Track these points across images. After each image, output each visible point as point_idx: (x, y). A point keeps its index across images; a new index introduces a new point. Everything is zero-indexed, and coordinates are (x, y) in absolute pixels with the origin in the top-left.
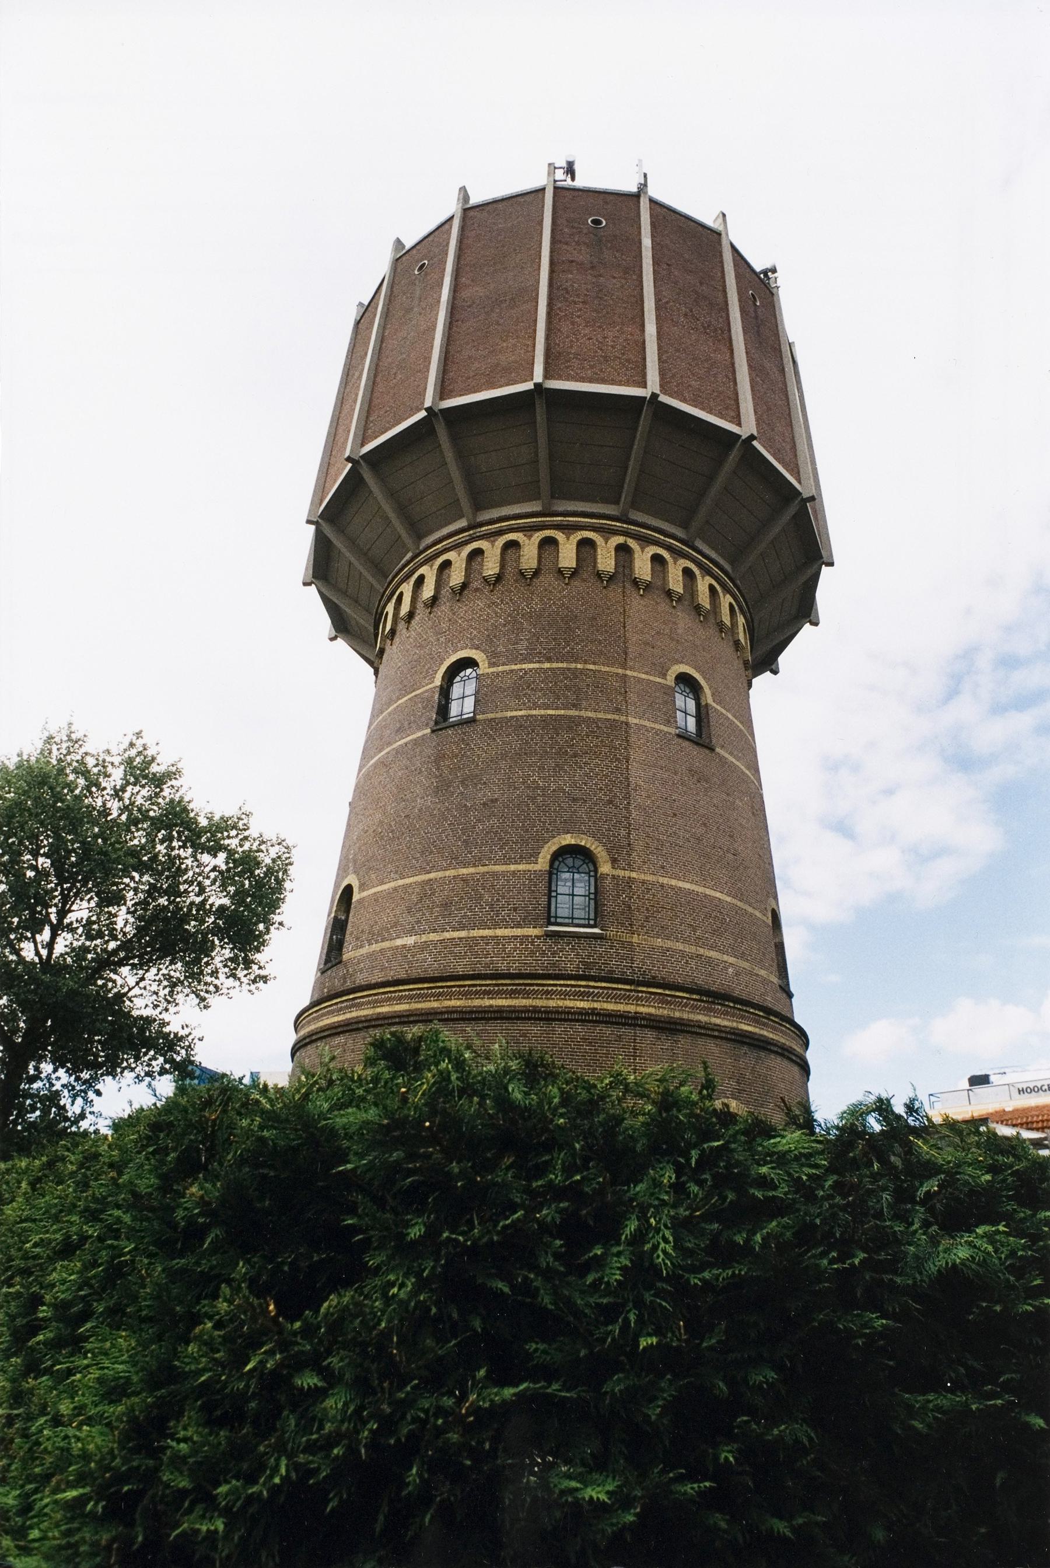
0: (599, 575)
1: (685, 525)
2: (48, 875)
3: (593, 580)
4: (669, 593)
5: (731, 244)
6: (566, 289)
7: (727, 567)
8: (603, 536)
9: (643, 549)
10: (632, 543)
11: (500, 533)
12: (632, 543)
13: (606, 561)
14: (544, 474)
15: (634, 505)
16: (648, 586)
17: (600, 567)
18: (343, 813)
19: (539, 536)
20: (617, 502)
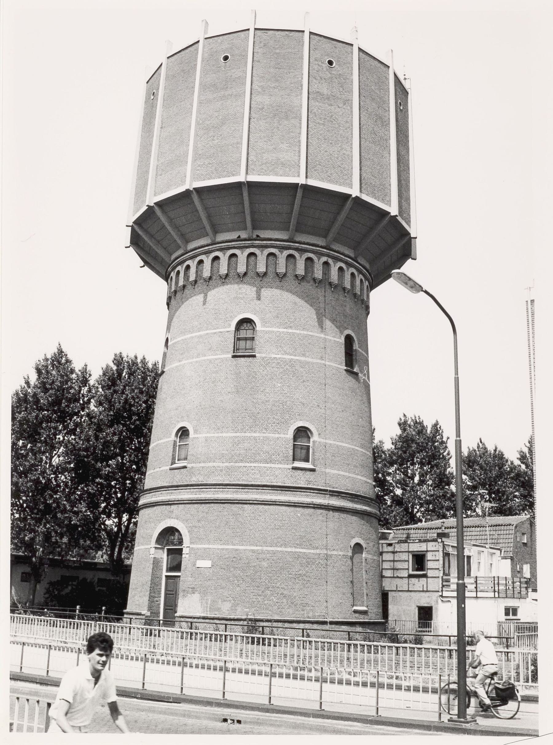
0: (314, 280)
1: (355, 248)
2: (141, 477)
3: (312, 282)
4: (344, 289)
5: (395, 75)
6: (315, 113)
7: (368, 266)
8: (317, 257)
9: (335, 264)
10: (330, 261)
11: (267, 247)
12: (330, 261)
13: (318, 274)
14: (293, 222)
15: (335, 240)
16: (336, 286)
17: (316, 276)
18: (483, 737)
19: (286, 253)
20: (325, 237)
